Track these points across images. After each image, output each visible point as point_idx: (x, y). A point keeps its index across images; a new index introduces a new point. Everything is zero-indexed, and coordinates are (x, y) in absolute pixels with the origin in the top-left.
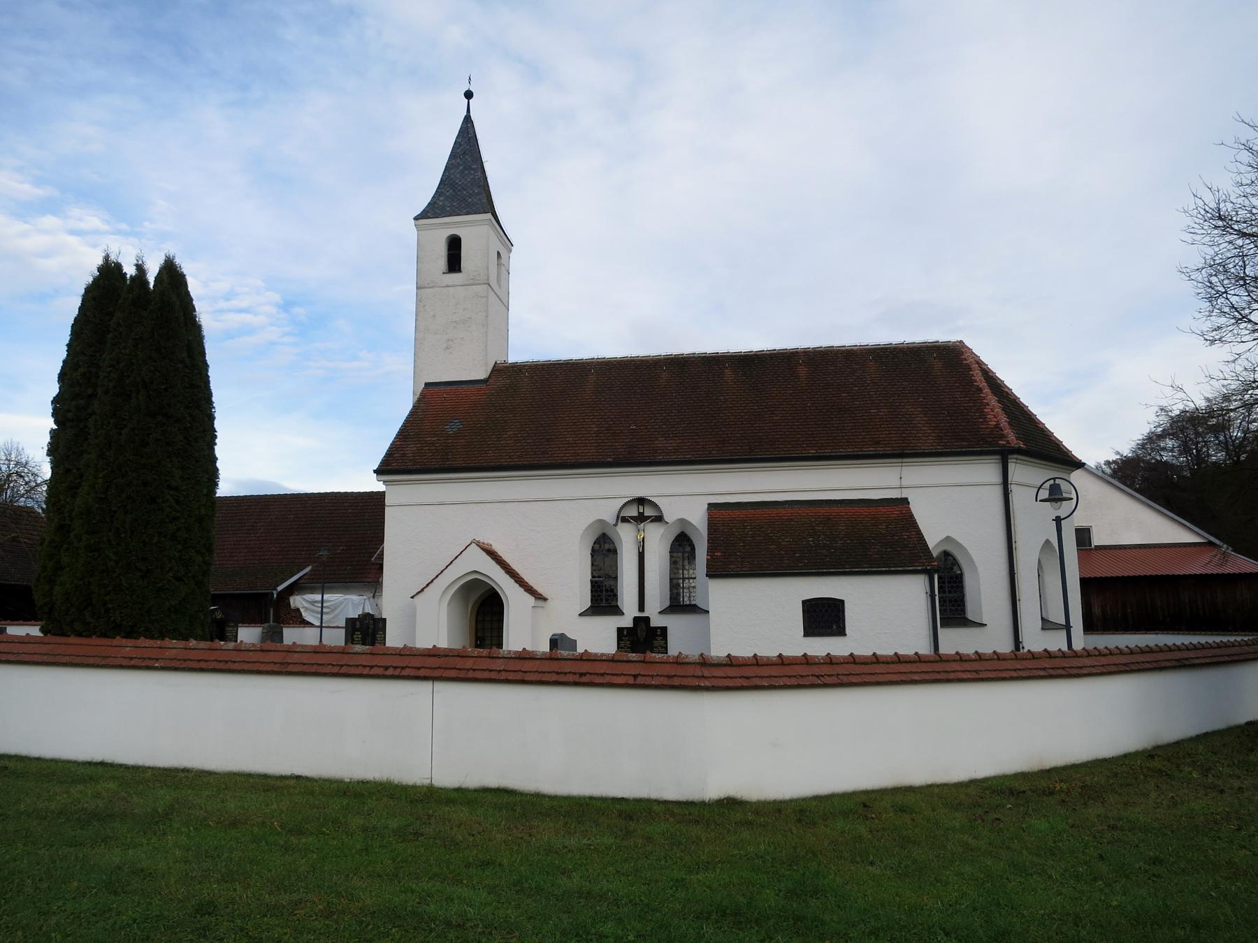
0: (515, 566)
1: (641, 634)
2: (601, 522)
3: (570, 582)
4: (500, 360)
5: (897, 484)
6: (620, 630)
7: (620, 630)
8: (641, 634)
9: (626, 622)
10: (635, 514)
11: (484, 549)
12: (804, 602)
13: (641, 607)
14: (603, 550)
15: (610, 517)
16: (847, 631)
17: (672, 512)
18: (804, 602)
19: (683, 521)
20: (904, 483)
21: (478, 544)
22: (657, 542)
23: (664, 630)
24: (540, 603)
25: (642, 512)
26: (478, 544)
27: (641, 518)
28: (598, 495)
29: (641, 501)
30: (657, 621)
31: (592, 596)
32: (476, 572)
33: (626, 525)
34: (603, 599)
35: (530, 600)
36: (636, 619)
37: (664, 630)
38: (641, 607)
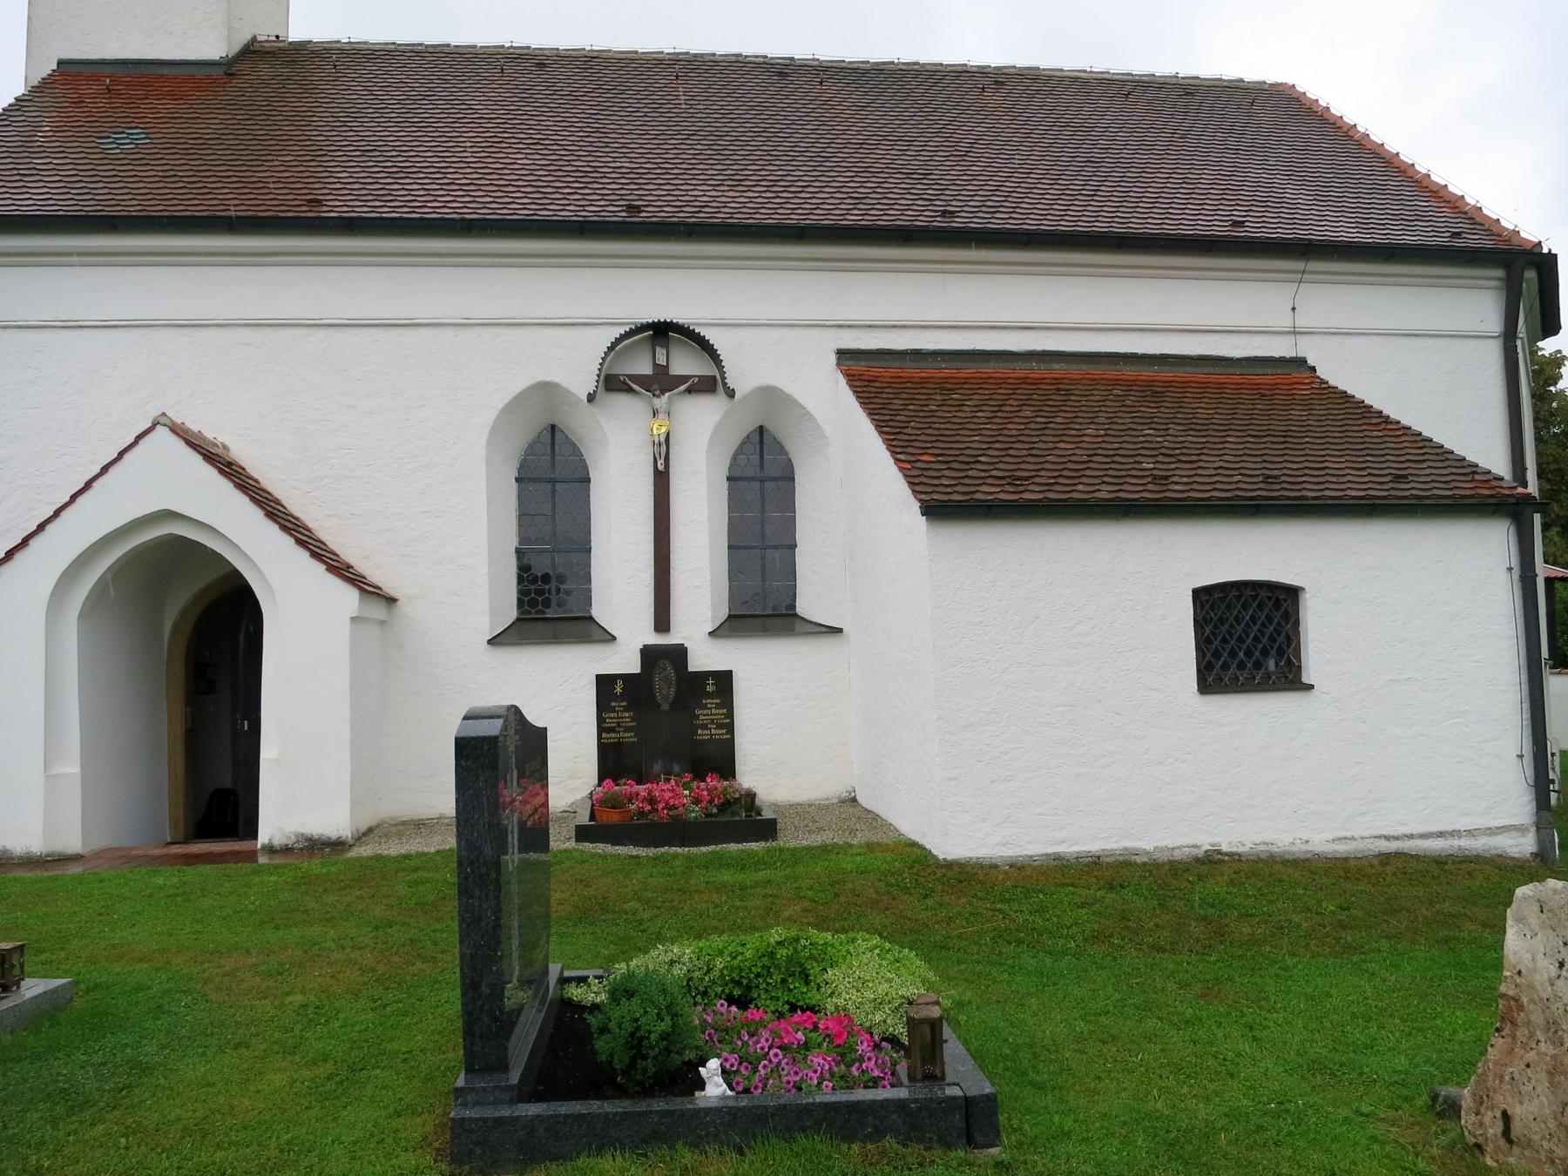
0: (296, 505)
1: (664, 691)
2: (546, 391)
3: (459, 561)
4: (265, 32)
5: (1285, 322)
6: (604, 683)
7: (604, 683)
8: (664, 691)
9: (624, 660)
10: (644, 368)
11: (189, 443)
12: (730, 672)
13: (662, 621)
14: (550, 478)
15: (580, 377)
16: (1314, 664)
17: (749, 362)
18: (730, 672)
19: (770, 395)
20: (1302, 321)
21: (178, 431)
22: (701, 434)
23: (724, 680)
24: (377, 611)
25: (663, 358)
26: (178, 431)
27: (661, 382)
28: (551, 318)
29: (662, 332)
30: (705, 657)
31: (522, 593)
32: (168, 515)
33: (622, 401)
34: (548, 600)
35: (348, 597)
36: (649, 655)
37: (724, 680)
38: (662, 621)
